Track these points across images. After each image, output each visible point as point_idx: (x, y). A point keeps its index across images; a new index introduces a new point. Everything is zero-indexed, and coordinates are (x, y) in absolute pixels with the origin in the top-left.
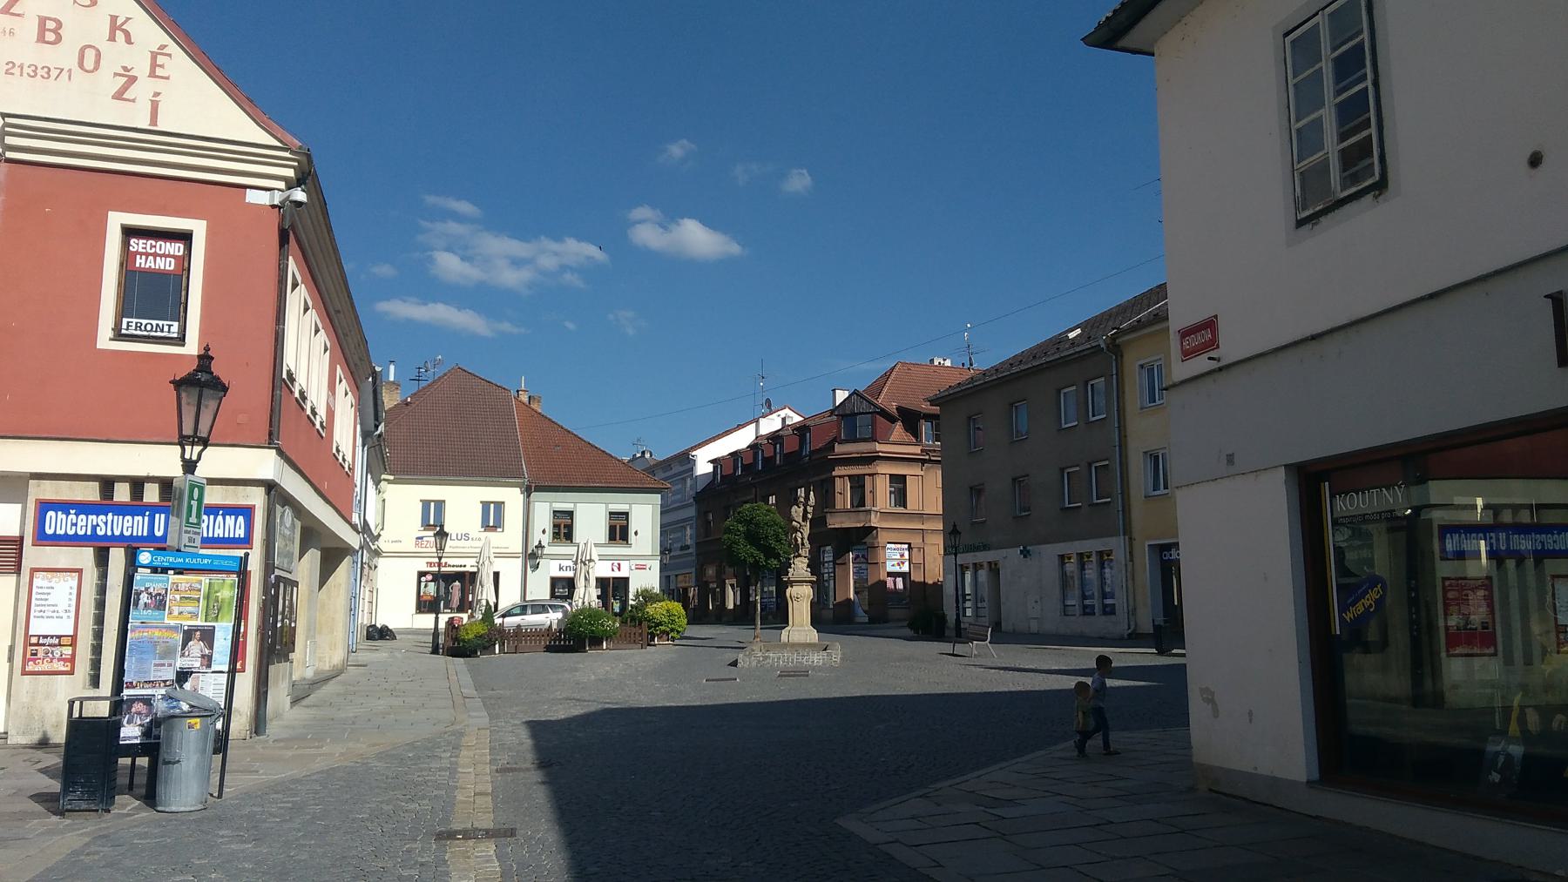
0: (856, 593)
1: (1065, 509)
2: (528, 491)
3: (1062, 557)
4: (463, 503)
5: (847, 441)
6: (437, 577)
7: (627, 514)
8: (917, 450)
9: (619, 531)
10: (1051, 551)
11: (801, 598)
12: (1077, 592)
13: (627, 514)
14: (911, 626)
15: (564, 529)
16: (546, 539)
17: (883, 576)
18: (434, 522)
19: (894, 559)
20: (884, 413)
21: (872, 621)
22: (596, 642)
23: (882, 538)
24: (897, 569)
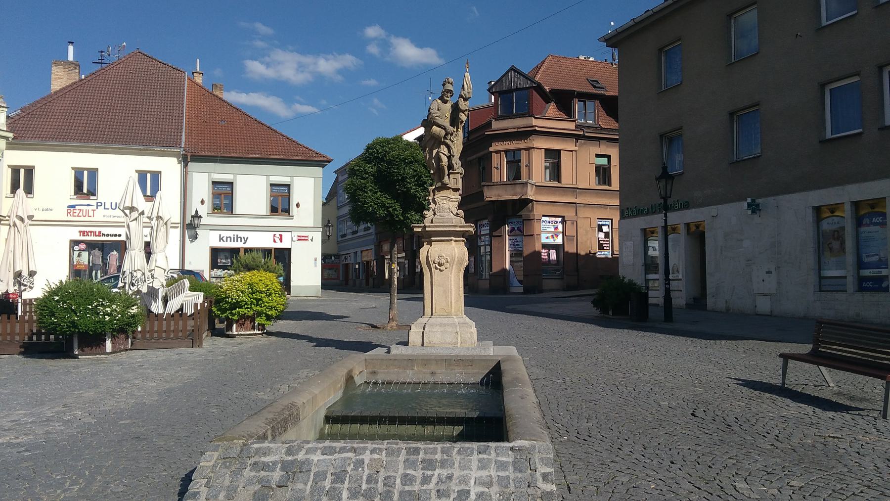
0: (511, 262)
1: (824, 142)
2: (185, 160)
3: (818, 210)
4: (117, 171)
5: (504, 118)
6: (91, 246)
7: (288, 186)
8: (571, 126)
9: (280, 203)
10: (794, 211)
11: (446, 262)
12: (850, 258)
13: (288, 186)
14: (595, 303)
15: (223, 198)
16: (204, 210)
17: (538, 247)
18: (85, 185)
19: (548, 232)
20: (539, 88)
21: (527, 291)
22: (92, 340)
23: (538, 210)
24: (551, 241)
